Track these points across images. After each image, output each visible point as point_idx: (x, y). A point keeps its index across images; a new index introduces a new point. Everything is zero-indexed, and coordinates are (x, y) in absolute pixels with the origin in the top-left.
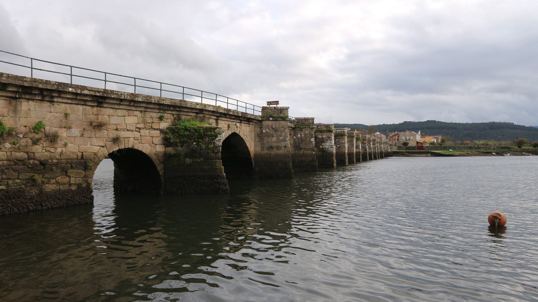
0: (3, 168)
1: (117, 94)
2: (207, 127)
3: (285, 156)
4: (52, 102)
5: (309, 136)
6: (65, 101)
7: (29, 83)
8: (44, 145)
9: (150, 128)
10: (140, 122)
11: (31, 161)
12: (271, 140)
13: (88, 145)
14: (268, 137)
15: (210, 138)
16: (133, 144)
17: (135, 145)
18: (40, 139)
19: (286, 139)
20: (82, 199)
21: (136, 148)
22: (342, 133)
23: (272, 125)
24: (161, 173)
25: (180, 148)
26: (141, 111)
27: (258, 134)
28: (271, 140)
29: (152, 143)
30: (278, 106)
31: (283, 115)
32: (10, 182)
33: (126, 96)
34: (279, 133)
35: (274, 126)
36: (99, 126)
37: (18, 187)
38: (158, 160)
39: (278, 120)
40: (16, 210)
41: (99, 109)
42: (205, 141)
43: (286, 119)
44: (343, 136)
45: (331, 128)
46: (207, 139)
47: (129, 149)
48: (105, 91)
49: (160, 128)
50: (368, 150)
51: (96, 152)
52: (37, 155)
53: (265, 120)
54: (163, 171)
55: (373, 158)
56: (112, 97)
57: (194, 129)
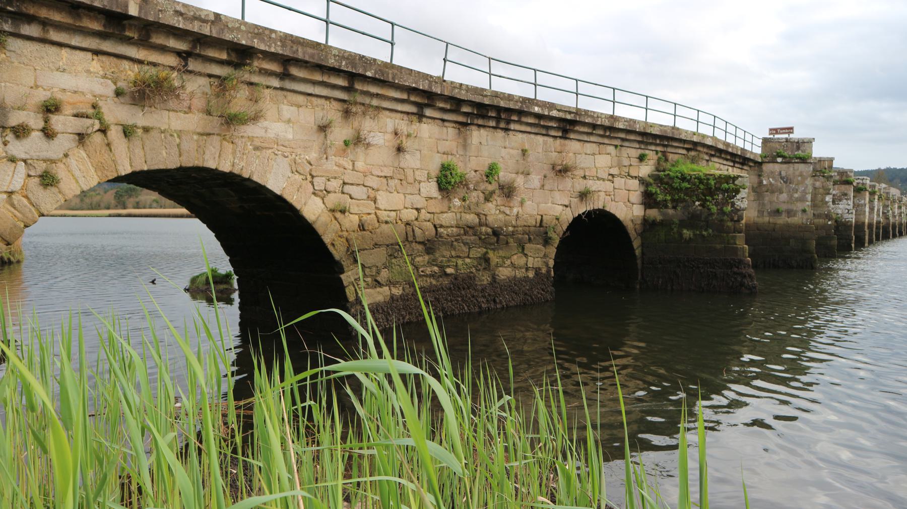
0: (453, 239)
1: (592, 117)
2: (720, 175)
3: (802, 228)
4: (506, 130)
5: (821, 191)
6: (523, 128)
7: (490, 99)
8: (499, 203)
9: (627, 174)
10: (614, 164)
11: (484, 229)
12: (777, 198)
13: (548, 203)
14: (773, 192)
15: (726, 194)
16: (604, 202)
17: (607, 205)
18: (493, 192)
19: (806, 198)
20: (541, 294)
21: (608, 210)
22: (860, 186)
23: (780, 172)
24: (638, 252)
25: (671, 212)
26: (616, 146)
27: (753, 187)
28: (777, 198)
29: (628, 201)
30: (791, 136)
31: (803, 154)
32: (460, 262)
33: (603, 120)
34: (794, 186)
35: (783, 174)
36: (562, 171)
37: (468, 271)
38: (635, 230)
39: (792, 163)
40: (466, 308)
41: (562, 141)
42: (717, 199)
43: (809, 161)
44: (862, 192)
45: (851, 177)
46: (721, 196)
47: (599, 210)
48: (578, 112)
49: (640, 175)
50: (891, 218)
51: (558, 214)
52: (490, 219)
53: (769, 162)
54: (640, 249)
55: (898, 235)
56: (587, 121)
57: (699, 178)
